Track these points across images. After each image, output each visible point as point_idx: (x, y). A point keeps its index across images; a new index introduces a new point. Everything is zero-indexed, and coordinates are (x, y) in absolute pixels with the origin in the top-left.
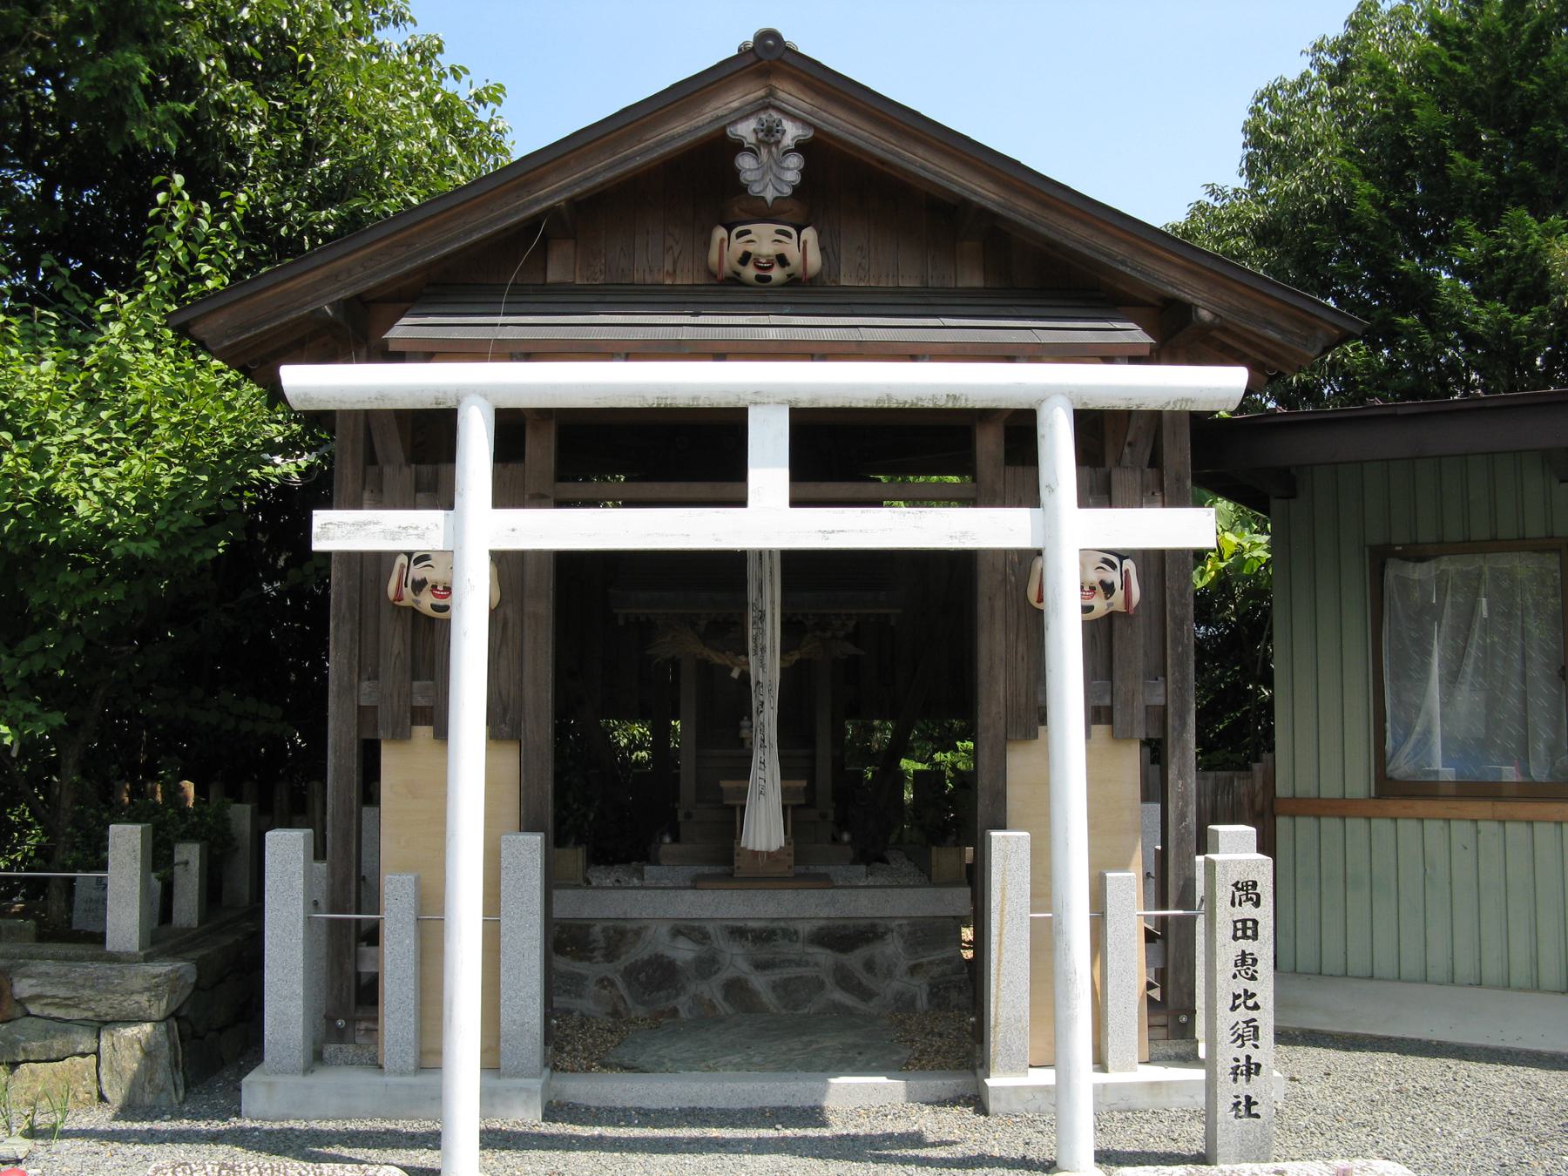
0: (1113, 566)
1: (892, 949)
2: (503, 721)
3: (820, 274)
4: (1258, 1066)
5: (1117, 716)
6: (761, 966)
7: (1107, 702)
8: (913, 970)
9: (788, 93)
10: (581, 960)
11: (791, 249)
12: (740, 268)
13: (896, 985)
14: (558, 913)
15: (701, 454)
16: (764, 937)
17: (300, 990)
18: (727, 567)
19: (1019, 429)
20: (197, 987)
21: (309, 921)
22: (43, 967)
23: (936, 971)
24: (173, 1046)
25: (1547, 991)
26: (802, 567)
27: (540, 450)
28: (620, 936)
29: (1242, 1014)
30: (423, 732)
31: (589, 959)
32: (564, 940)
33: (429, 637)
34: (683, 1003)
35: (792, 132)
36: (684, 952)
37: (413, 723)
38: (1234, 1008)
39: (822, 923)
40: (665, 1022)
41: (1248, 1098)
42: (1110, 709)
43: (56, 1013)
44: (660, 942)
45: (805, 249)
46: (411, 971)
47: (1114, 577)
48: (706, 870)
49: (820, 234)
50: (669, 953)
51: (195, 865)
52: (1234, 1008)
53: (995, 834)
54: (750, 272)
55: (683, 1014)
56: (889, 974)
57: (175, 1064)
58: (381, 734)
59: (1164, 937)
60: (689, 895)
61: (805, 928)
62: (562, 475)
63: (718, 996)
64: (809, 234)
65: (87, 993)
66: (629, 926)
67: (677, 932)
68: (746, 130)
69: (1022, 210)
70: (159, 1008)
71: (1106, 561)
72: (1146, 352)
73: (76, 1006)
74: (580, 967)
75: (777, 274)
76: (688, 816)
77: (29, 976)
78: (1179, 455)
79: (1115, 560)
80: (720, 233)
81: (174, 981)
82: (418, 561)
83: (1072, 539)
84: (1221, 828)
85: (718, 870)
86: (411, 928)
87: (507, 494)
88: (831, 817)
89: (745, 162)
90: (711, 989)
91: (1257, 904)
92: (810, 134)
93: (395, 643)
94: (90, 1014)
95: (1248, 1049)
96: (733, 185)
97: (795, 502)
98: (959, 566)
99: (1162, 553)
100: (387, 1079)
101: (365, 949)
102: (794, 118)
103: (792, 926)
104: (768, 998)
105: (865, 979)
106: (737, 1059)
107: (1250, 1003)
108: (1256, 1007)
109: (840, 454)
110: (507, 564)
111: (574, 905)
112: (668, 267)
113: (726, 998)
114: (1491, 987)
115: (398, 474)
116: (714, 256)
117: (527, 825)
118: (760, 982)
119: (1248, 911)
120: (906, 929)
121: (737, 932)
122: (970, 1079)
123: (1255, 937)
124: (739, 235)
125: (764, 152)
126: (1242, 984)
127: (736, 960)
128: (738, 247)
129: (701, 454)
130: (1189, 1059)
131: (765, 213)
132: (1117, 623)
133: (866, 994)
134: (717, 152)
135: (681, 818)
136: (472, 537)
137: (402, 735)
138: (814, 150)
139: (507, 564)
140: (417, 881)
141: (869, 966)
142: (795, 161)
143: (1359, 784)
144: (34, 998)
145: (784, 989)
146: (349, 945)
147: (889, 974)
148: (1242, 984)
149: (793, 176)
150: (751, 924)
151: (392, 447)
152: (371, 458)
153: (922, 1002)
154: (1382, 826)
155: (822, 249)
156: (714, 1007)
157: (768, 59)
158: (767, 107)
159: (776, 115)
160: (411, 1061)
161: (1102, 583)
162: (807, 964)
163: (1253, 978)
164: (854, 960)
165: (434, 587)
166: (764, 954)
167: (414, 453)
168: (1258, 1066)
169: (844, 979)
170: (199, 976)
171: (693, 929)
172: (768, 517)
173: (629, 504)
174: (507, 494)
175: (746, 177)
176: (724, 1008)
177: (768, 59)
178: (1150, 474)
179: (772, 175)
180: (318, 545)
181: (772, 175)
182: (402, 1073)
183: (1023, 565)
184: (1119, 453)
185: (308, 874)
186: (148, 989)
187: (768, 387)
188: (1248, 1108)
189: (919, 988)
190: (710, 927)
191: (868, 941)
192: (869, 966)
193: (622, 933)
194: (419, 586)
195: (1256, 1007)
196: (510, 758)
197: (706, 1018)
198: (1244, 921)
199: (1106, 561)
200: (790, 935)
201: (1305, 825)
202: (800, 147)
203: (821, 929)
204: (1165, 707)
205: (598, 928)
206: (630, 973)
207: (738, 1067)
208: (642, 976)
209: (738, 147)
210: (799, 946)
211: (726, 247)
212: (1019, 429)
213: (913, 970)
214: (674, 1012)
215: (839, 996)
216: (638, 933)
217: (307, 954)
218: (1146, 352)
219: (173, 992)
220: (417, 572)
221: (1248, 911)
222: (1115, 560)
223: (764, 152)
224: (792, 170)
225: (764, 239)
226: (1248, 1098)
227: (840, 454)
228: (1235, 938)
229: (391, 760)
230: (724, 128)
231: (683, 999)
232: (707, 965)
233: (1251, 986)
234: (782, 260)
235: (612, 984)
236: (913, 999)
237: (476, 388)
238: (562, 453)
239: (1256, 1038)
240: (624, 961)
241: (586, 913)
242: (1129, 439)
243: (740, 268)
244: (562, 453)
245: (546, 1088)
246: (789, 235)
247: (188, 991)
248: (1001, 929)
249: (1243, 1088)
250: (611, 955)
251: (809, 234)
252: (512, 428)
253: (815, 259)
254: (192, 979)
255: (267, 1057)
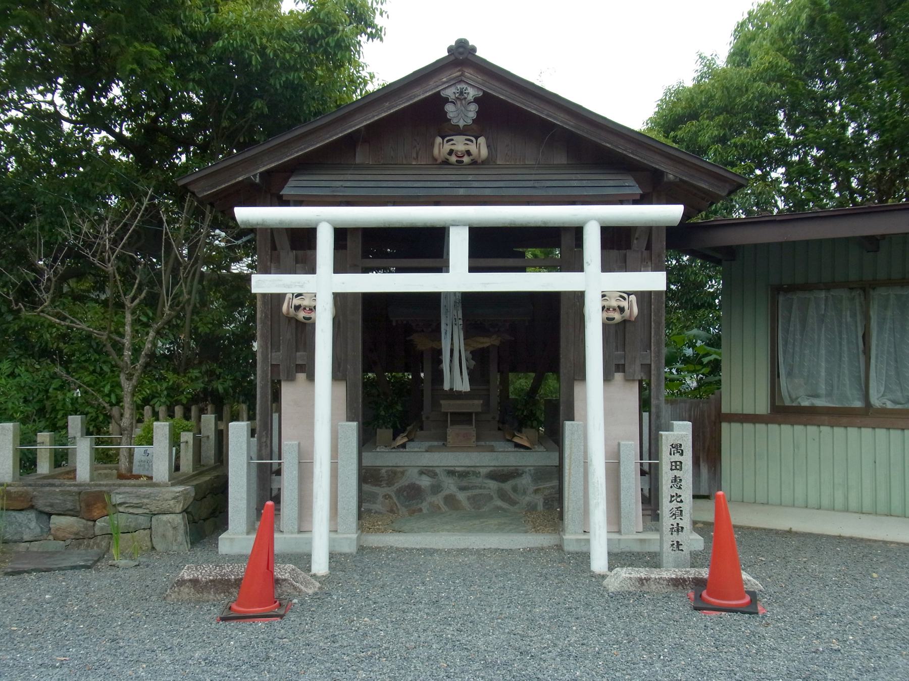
0: (624, 299)
1: (525, 481)
2: (338, 373)
3: (487, 158)
4: (682, 528)
5: (626, 369)
6: (462, 489)
7: (622, 362)
8: (536, 491)
9: (469, 73)
10: (376, 486)
11: (472, 148)
12: (448, 157)
13: (528, 499)
14: (365, 463)
15: (426, 247)
16: (463, 475)
17: (245, 496)
18: (432, 300)
19: (574, 234)
20: (195, 499)
21: (249, 464)
22: (122, 489)
23: (547, 492)
24: (185, 525)
25: (880, 515)
26: (469, 300)
27: (355, 245)
28: (394, 474)
29: (675, 504)
30: (301, 377)
31: (380, 486)
32: (367, 476)
33: (303, 331)
34: (425, 506)
35: (472, 93)
36: (425, 482)
37: (297, 372)
38: (671, 502)
39: (492, 469)
40: (415, 512)
41: (678, 542)
42: (624, 365)
43: (131, 510)
44: (412, 476)
45: (480, 148)
46: (296, 486)
47: (624, 304)
48: (436, 443)
49: (487, 139)
50: (417, 482)
51: (191, 442)
52: (671, 502)
53: (568, 423)
54: (453, 159)
55: (425, 511)
56: (525, 493)
57: (186, 533)
58: (282, 377)
59: (649, 473)
60: (427, 454)
61: (484, 471)
62: (365, 255)
63: (441, 504)
64: (482, 140)
65: (146, 501)
66: (398, 469)
67: (421, 473)
68: (450, 93)
69: (583, 131)
70: (179, 508)
71: (621, 296)
72: (638, 197)
73: (140, 507)
74: (375, 489)
75: (466, 159)
76: (427, 418)
77: (119, 494)
78: (660, 244)
79: (625, 296)
80: (439, 140)
81: (185, 494)
82: (297, 296)
83: (599, 287)
84: (675, 422)
85: (441, 443)
86: (296, 467)
87: (340, 267)
88: (497, 419)
89: (449, 108)
90: (438, 500)
91: (682, 454)
92: (481, 94)
93: (287, 334)
94: (147, 511)
95: (678, 520)
96: (443, 117)
97: (472, 269)
98: (552, 299)
99: (650, 293)
100: (284, 536)
101: (274, 477)
102: (473, 86)
103: (477, 470)
104: (465, 503)
105: (513, 496)
106: (448, 527)
107: (679, 500)
108: (681, 501)
109: (491, 247)
110: (340, 299)
111: (371, 459)
112: (414, 155)
113: (445, 503)
114: (838, 511)
115: (288, 256)
116: (436, 151)
117: (350, 419)
118: (461, 496)
119: (677, 457)
120: (533, 472)
121: (451, 473)
122: (557, 536)
123: (681, 469)
124: (448, 141)
125: (459, 103)
126: (675, 491)
127: (450, 486)
128: (447, 147)
129: (426, 247)
130: (658, 530)
131: (458, 131)
132: (628, 325)
133: (513, 503)
134: (437, 102)
135: (424, 419)
136: (321, 288)
137: (291, 378)
138: (484, 101)
139: (340, 299)
140: (299, 444)
141: (515, 489)
142: (474, 107)
143: (762, 407)
144: (121, 504)
145: (473, 500)
146: (267, 478)
147: (525, 493)
148: (675, 491)
149: (472, 115)
150: (457, 469)
151: (284, 243)
152: (274, 248)
153: (540, 507)
154: (774, 427)
155: (488, 146)
156: (439, 508)
157: (462, 57)
158: (461, 81)
159: (465, 86)
160: (296, 527)
161: (619, 307)
162: (485, 488)
163: (680, 488)
164: (507, 486)
165: (305, 309)
166: (464, 483)
167: (297, 246)
168: (682, 528)
169: (503, 495)
170: (196, 494)
171: (429, 471)
172: (458, 277)
173: (400, 270)
174: (340, 267)
175: (450, 115)
176: (444, 508)
177: (462, 57)
178: (646, 253)
179: (462, 114)
180: (253, 291)
181: (462, 114)
182: (292, 533)
183: (579, 298)
184: (620, 244)
185: (248, 443)
186: (173, 499)
187: (459, 219)
188: (678, 547)
189: (539, 500)
190: (437, 470)
191: (514, 477)
192: (515, 489)
193: (395, 473)
194: (297, 308)
195: (681, 501)
196: (342, 388)
197: (435, 511)
198: (676, 462)
199: (621, 296)
200: (477, 474)
201: (736, 426)
202: (477, 100)
203: (491, 471)
204: (650, 365)
205: (383, 471)
206: (399, 492)
207: (449, 531)
208: (405, 493)
209: (446, 100)
210: (480, 480)
211: (441, 148)
212: (574, 234)
213: (536, 491)
214: (420, 510)
215: (499, 503)
216: (403, 473)
217: (249, 480)
218: (638, 197)
219: (185, 500)
220: (296, 302)
221: (677, 457)
222: (625, 296)
223: (459, 103)
224: (473, 109)
225: (460, 144)
226: (678, 542)
227: (491, 247)
228: (671, 469)
229: (288, 392)
230: (439, 92)
231: (424, 504)
232: (436, 489)
233: (679, 492)
234: (468, 153)
235: (390, 497)
236: (536, 505)
237: (325, 219)
238: (364, 248)
239: (681, 515)
240: (397, 486)
241: (378, 463)
242: (636, 236)
243: (448, 157)
244: (364, 248)
245: (358, 539)
246: (472, 141)
247: (192, 500)
248: (570, 466)
249: (675, 537)
250: (390, 483)
251: (482, 140)
252: (342, 235)
253: (484, 152)
254: (193, 494)
255: (230, 527)
